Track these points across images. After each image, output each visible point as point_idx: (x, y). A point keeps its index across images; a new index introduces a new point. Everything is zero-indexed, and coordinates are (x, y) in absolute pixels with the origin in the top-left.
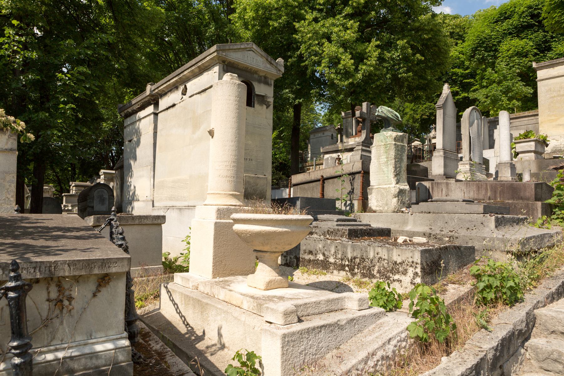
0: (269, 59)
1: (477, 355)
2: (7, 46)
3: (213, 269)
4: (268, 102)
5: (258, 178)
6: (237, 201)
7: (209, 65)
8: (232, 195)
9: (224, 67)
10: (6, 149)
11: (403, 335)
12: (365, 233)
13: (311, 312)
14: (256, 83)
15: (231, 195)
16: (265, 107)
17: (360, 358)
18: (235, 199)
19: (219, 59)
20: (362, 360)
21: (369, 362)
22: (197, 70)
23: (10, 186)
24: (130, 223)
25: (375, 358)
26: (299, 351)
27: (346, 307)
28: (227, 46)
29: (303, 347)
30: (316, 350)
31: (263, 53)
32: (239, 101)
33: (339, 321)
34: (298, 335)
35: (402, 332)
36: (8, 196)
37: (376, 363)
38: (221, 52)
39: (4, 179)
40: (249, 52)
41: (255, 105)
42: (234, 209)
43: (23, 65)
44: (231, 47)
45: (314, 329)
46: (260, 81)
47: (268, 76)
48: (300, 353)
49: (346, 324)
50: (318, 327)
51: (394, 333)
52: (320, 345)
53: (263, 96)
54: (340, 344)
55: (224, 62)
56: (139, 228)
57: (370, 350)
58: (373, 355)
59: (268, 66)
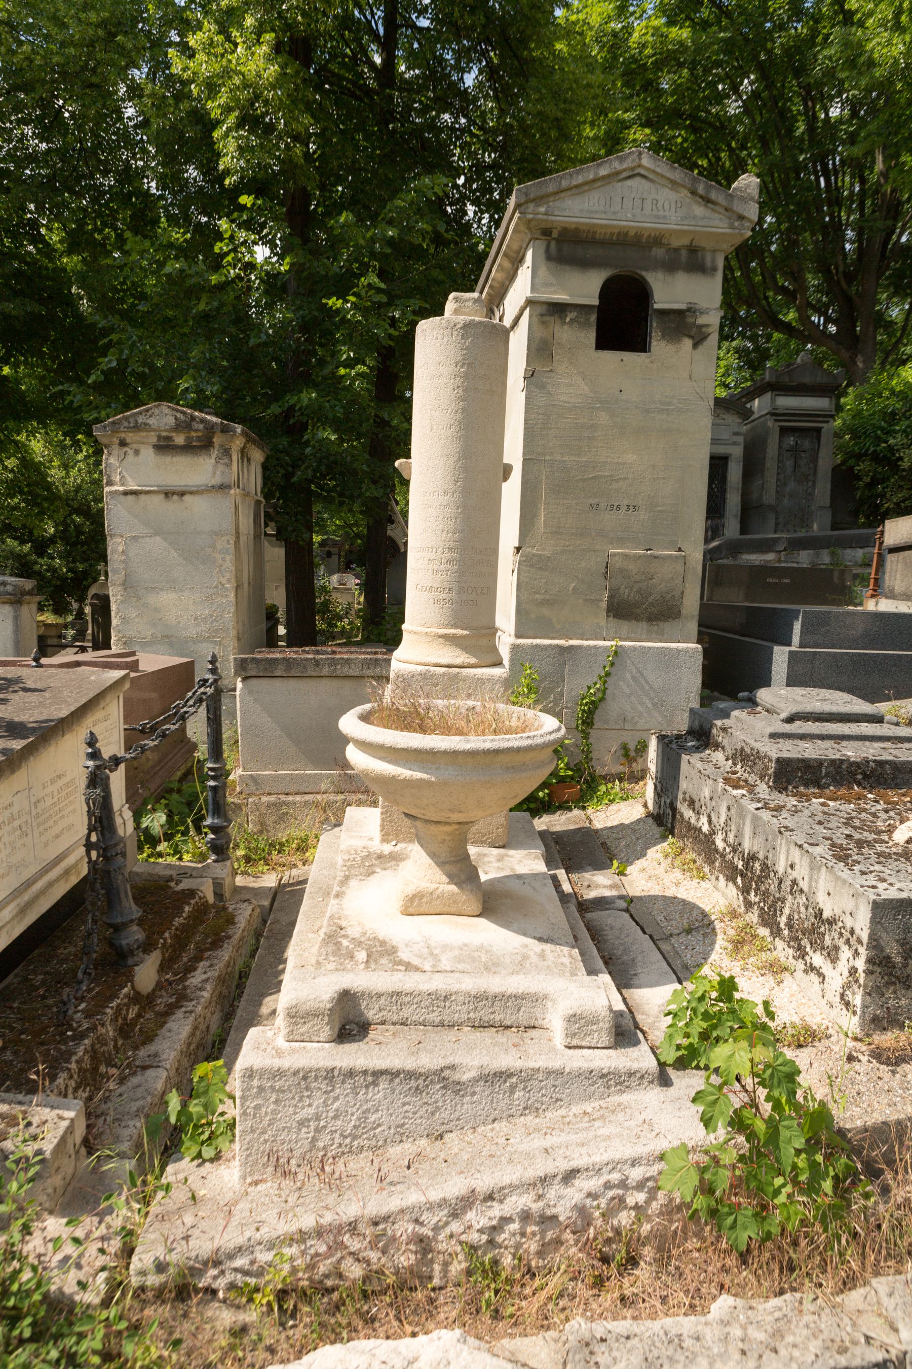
0: (701, 190)
1: (843, 1351)
2: (229, 258)
3: (383, 820)
4: (701, 327)
5: (656, 557)
6: (458, 651)
7: (521, 248)
8: (445, 637)
9: (548, 247)
10: (213, 487)
11: (636, 1174)
12: (853, 774)
13: (415, 1018)
14: (660, 275)
15: (441, 636)
16: (688, 343)
17: (435, 1195)
18: (452, 648)
19: (530, 229)
20: (443, 1203)
21: (470, 1215)
22: (507, 264)
23: (224, 559)
24: (309, 673)
25: (496, 1211)
26: (298, 1117)
27: (546, 1023)
28: (549, 184)
29: (312, 1111)
30: (355, 1127)
31: (678, 174)
32: (466, 376)
33: (453, 1067)
34: (292, 1081)
35: (634, 1163)
36: (221, 579)
37: (494, 1222)
38: (531, 206)
39: (213, 546)
40: (629, 183)
41: (654, 343)
42: (444, 675)
43: (266, 292)
44: (565, 184)
45: (351, 1073)
46: (671, 265)
47: (703, 243)
48: (302, 1123)
49: (475, 1080)
50: (365, 1072)
51: (599, 1158)
52: (373, 1118)
53: (680, 313)
54: (444, 1128)
55: (546, 232)
56: (335, 683)
57: (484, 1182)
58: (490, 1197)
59: (699, 210)
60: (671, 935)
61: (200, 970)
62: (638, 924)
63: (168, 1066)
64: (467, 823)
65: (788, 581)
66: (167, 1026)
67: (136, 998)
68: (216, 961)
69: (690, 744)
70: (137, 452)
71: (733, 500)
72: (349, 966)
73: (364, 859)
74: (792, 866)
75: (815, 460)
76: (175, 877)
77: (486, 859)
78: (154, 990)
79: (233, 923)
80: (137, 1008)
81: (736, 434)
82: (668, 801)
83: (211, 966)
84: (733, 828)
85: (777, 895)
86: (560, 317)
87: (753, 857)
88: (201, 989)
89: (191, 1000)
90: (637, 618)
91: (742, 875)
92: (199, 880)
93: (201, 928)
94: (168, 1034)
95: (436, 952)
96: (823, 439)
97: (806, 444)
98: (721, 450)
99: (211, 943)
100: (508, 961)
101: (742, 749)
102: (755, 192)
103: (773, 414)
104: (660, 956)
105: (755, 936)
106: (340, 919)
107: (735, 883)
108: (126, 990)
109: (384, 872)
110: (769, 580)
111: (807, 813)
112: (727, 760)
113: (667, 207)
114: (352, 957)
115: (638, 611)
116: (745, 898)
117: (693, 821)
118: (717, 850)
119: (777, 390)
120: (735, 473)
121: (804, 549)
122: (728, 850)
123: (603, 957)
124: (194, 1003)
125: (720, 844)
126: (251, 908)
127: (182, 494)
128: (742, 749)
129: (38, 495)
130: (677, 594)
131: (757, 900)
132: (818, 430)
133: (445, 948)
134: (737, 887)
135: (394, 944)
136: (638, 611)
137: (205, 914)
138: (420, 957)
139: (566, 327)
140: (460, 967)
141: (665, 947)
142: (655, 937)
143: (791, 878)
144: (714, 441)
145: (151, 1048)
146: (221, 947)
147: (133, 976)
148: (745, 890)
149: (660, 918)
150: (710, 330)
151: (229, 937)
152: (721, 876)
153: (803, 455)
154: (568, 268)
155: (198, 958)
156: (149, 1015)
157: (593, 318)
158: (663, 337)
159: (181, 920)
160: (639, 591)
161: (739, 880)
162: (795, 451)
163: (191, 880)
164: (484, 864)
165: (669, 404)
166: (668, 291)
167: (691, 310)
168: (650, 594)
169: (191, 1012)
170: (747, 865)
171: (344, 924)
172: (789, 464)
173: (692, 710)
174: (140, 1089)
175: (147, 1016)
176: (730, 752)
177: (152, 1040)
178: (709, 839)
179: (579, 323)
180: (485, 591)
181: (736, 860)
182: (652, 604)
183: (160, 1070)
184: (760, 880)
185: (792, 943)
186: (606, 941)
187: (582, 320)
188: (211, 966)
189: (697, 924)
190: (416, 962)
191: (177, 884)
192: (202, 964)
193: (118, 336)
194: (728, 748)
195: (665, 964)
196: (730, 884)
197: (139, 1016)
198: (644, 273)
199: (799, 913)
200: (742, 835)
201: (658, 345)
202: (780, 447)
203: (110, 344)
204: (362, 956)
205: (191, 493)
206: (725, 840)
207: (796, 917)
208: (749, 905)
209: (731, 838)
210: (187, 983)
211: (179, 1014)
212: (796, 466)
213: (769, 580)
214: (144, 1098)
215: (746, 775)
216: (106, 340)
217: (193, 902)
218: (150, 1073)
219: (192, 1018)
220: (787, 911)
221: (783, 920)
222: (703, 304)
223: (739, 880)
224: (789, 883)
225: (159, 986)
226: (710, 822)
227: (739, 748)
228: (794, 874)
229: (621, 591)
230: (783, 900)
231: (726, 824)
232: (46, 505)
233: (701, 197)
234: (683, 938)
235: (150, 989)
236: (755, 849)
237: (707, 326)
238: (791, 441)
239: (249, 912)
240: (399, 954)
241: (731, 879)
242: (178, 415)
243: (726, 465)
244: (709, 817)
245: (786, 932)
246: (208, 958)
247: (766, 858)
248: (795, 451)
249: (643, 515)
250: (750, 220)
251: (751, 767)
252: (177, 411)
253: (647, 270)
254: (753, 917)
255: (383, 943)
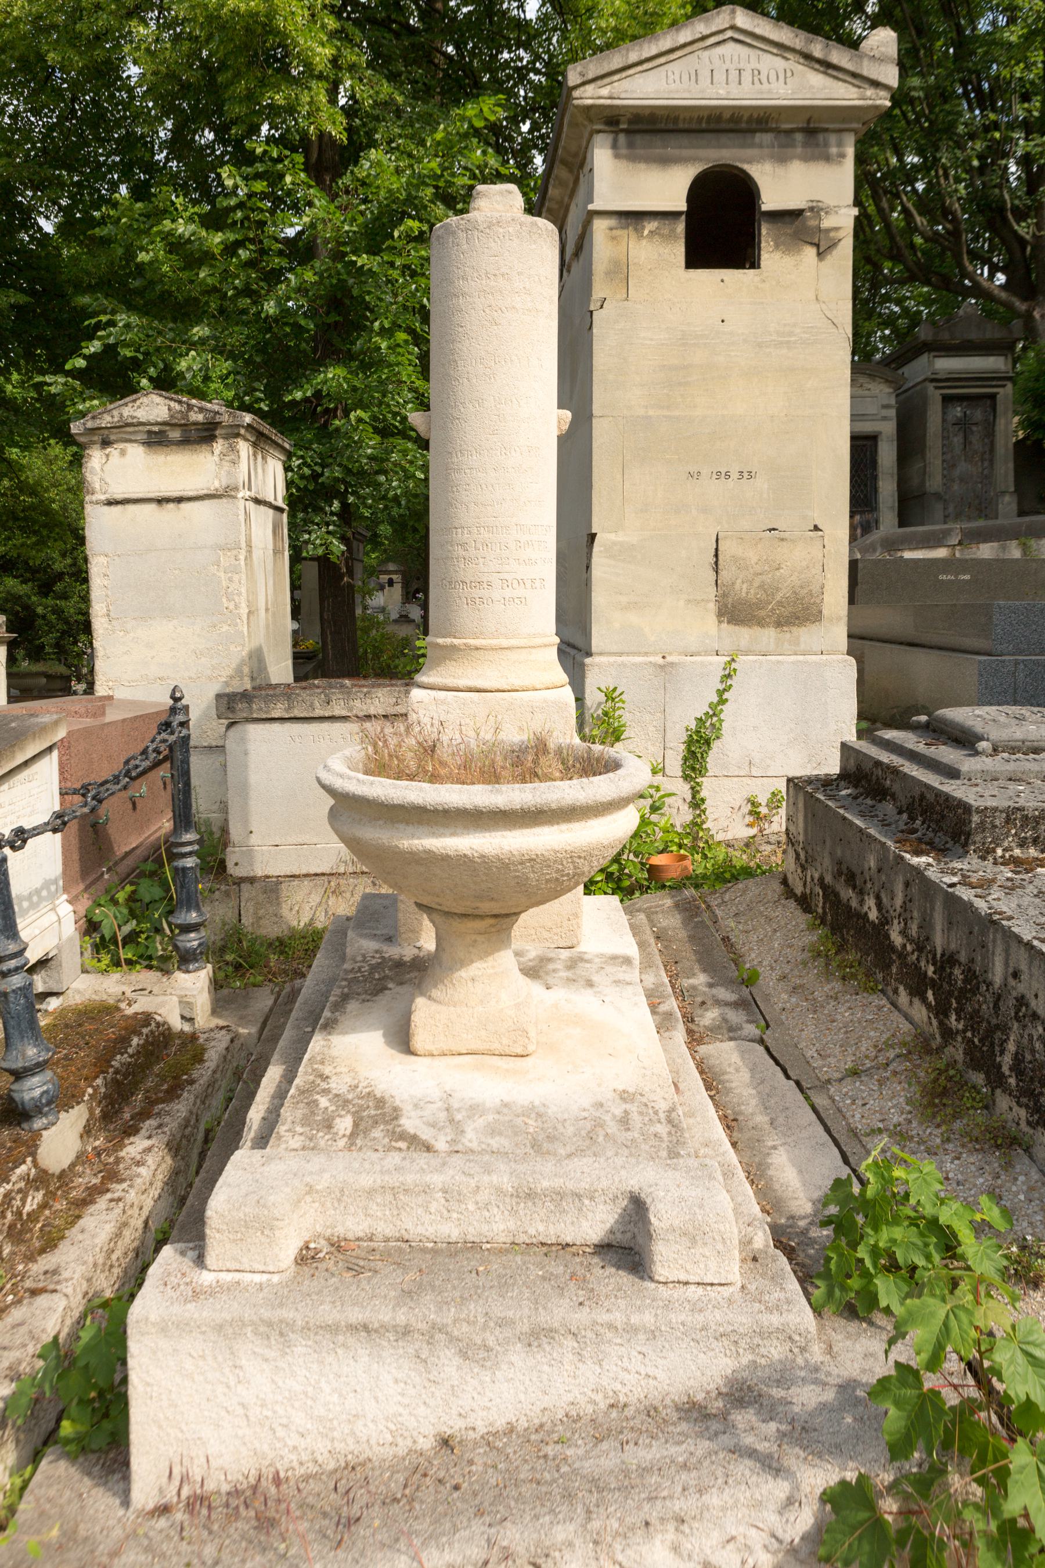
4: (828, 231)
16: (810, 252)
24: (318, 712)
60: (829, 1081)
61: (143, 1132)
62: (777, 1063)
63: (69, 1291)
64: (507, 915)
65: (967, 577)
66: (81, 1222)
67: (41, 1179)
68: (167, 1119)
69: (844, 793)
70: (123, 453)
71: (887, 489)
72: (322, 1143)
73: (374, 968)
74: (1016, 975)
75: (990, 431)
76: (128, 994)
77: (551, 966)
78: (73, 1165)
79: (201, 1061)
80: (39, 1196)
81: (886, 407)
82: (816, 876)
83: (160, 1126)
84: (915, 914)
85: (994, 1021)
86: (636, 229)
87: (949, 960)
88: (138, 1164)
89: (123, 1180)
90: (761, 623)
91: (933, 988)
92: (161, 998)
93: (156, 1069)
94: (80, 1237)
95: (458, 1117)
96: (1000, 408)
97: (978, 415)
98: (867, 427)
99: (167, 1092)
100: (570, 1130)
101: (922, 797)
102: (893, 50)
103: (933, 380)
104: (814, 1117)
105: (963, 1084)
106: (322, 1063)
107: (924, 1000)
108: (23, 1168)
109: (399, 989)
110: (942, 577)
111: (1030, 889)
112: (900, 813)
113: (773, 77)
114: (330, 1127)
115: (763, 613)
116: (941, 1023)
117: (854, 904)
118: (892, 948)
119: (934, 350)
120: (887, 455)
121: (985, 541)
122: (909, 948)
123: (723, 1118)
124: (125, 1185)
125: (897, 939)
126: (228, 1038)
127: (180, 500)
128: (922, 797)
129: (35, 522)
130: (815, 588)
131: (960, 1027)
132: (993, 397)
133: (475, 1110)
134: (928, 1006)
135: (398, 1103)
136: (763, 613)
137: (165, 1047)
138: (433, 1125)
139: (644, 242)
140: (495, 1142)
141: (820, 1101)
142: (804, 1084)
143: (1014, 994)
144: (855, 417)
145: (45, 1262)
146: (179, 1097)
147: (37, 1147)
148: (940, 1011)
149: (810, 1053)
150: (841, 234)
151: (192, 1082)
152: (901, 988)
153: (974, 428)
154: (642, 166)
155: (144, 1115)
156: (60, 1205)
157: (681, 227)
158: (777, 246)
159: (125, 1058)
160: (761, 586)
161: (930, 995)
162: (964, 425)
163: (151, 998)
164: (547, 973)
165: (791, 334)
166: (779, 185)
167: (816, 210)
168: (778, 589)
169: (119, 1199)
170: (940, 970)
171: (327, 1070)
172: (957, 440)
173: (844, 745)
174: (23, 1330)
175: (57, 1206)
176: (904, 802)
177: (56, 1246)
178: (880, 929)
179: (662, 236)
180: (538, 584)
181: (923, 964)
182: (780, 603)
183: (55, 1297)
184: (964, 995)
185: (1024, 1100)
186: (729, 1091)
187: (666, 232)
188: (160, 1126)
189: (868, 1064)
190: (425, 1134)
191: (129, 1005)
192: (148, 1122)
193: (108, 317)
194: (900, 795)
195: (820, 1129)
196: (916, 1001)
197: (44, 1206)
198: (746, 167)
199: (1033, 1051)
200: (932, 927)
201: (769, 256)
202: (944, 420)
203: (98, 326)
204: (344, 1124)
205: (190, 499)
206: (903, 933)
207: (1028, 1057)
208: (948, 1034)
209: (914, 930)
210: (122, 1154)
211: (102, 1202)
212: (966, 442)
213: (942, 577)
214: (25, 1346)
215: (931, 834)
216: (93, 321)
217: (145, 1031)
218: (42, 1300)
219: (118, 1211)
220: (1011, 1047)
221: (1006, 1061)
222: (829, 201)
223: (930, 995)
224: (1012, 1002)
225: (81, 1158)
226: (879, 905)
227: (917, 795)
228: (1021, 988)
229: (737, 587)
230: (1005, 1029)
231: (904, 906)
232: (45, 533)
233: (819, 61)
234: (847, 1087)
235: (65, 1164)
236: (953, 946)
237: (837, 229)
238: (958, 411)
239: (224, 1044)
240: (403, 1121)
241: (917, 991)
242: (172, 404)
243: (876, 446)
244: (878, 898)
245: (1012, 1081)
246: (158, 1114)
247: (972, 961)
248: (964, 425)
249: (761, 483)
250: (886, 87)
251: (937, 822)
252: (172, 399)
253: (750, 162)
254: (957, 1052)
255: (380, 1102)
